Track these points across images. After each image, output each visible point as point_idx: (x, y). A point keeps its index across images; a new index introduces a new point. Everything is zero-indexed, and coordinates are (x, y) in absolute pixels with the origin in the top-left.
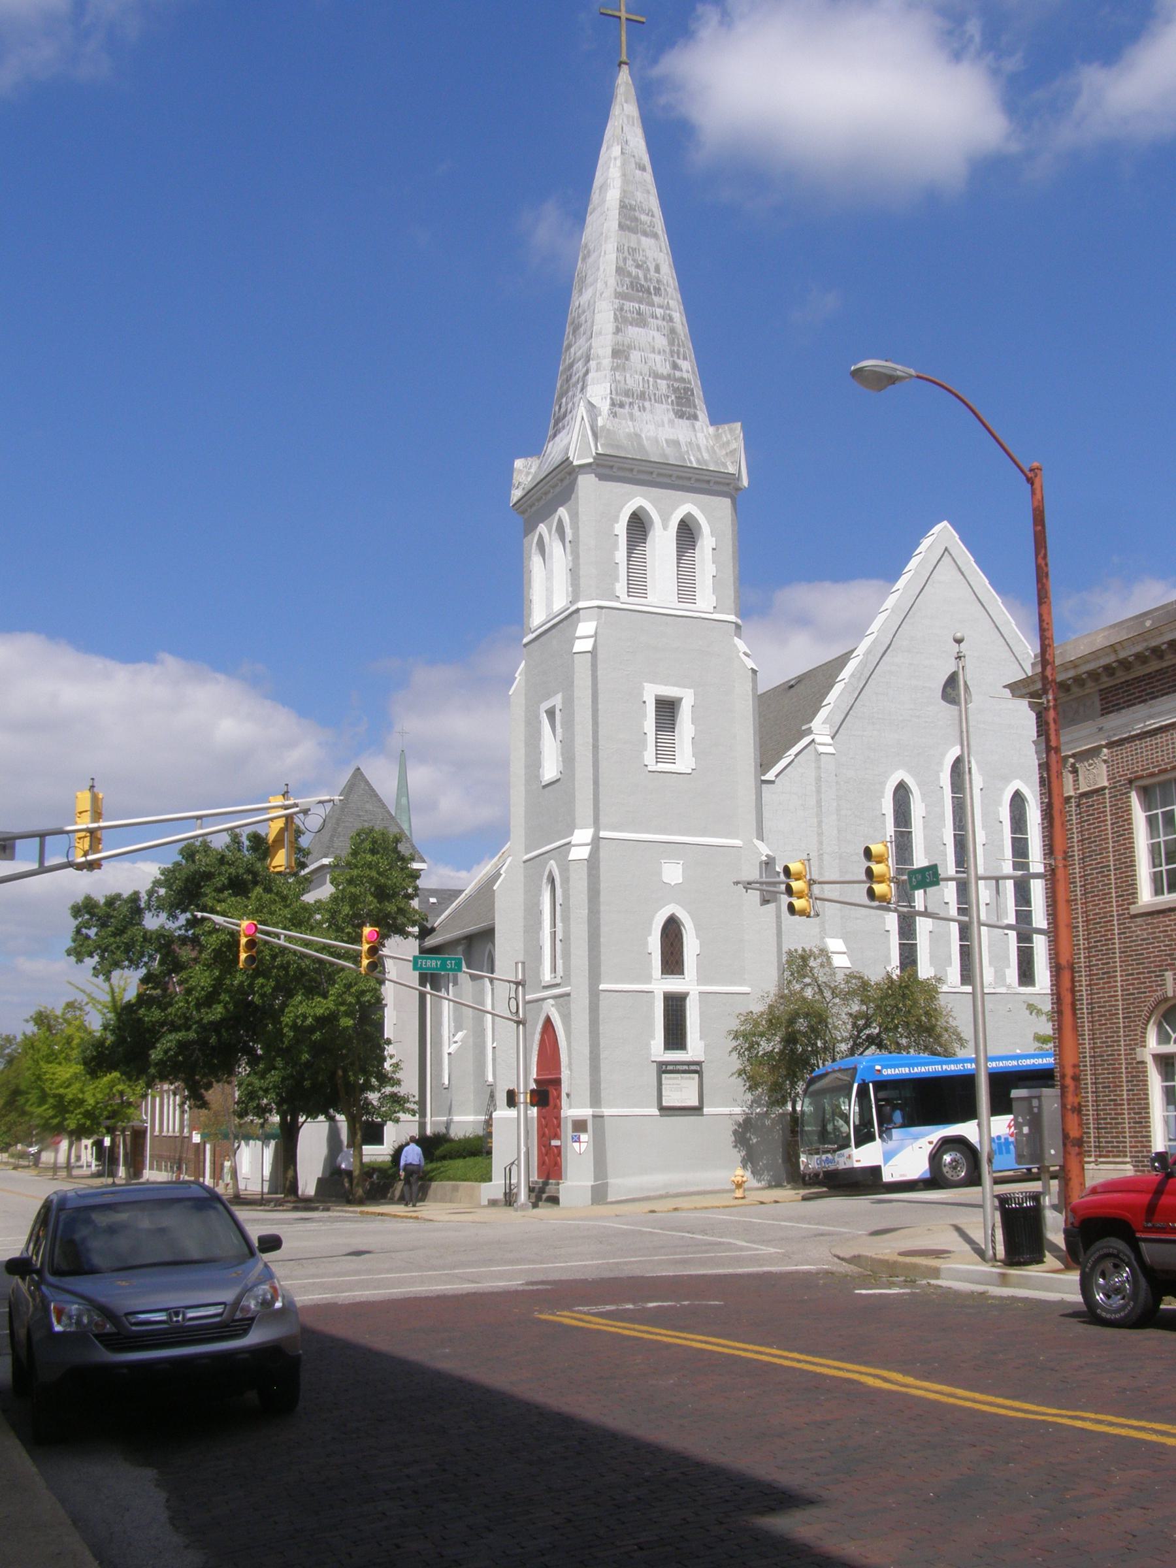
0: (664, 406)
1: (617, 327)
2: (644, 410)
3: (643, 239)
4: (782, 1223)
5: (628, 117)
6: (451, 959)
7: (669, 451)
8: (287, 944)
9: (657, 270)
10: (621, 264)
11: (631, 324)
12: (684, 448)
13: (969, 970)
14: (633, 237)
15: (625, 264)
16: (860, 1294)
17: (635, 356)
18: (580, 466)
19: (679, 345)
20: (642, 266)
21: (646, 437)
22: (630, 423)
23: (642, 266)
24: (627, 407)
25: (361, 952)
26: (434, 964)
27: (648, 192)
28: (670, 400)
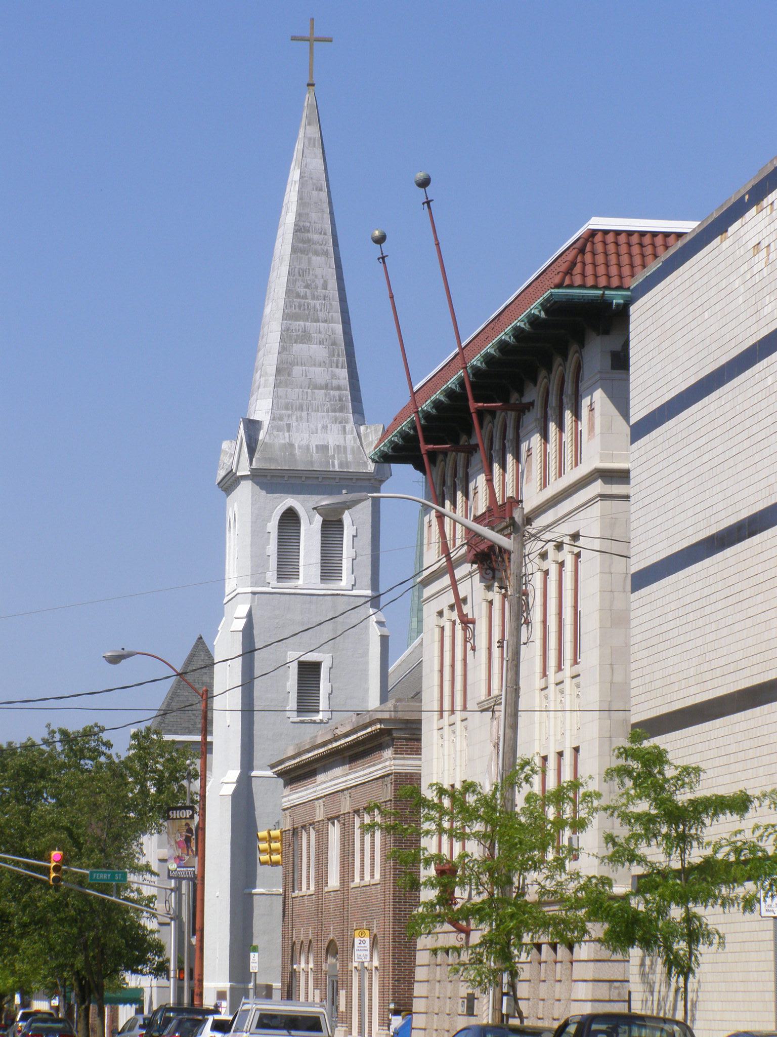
0: (320, 414)
1: (283, 347)
2: (301, 420)
3: (314, 258)
5: (310, 139)
7: (316, 456)
9: (325, 287)
11: (296, 342)
12: (331, 452)
14: (305, 258)
17: (297, 370)
18: (242, 476)
21: (299, 446)
22: (287, 434)
24: (286, 419)
26: (105, 876)
28: (325, 408)
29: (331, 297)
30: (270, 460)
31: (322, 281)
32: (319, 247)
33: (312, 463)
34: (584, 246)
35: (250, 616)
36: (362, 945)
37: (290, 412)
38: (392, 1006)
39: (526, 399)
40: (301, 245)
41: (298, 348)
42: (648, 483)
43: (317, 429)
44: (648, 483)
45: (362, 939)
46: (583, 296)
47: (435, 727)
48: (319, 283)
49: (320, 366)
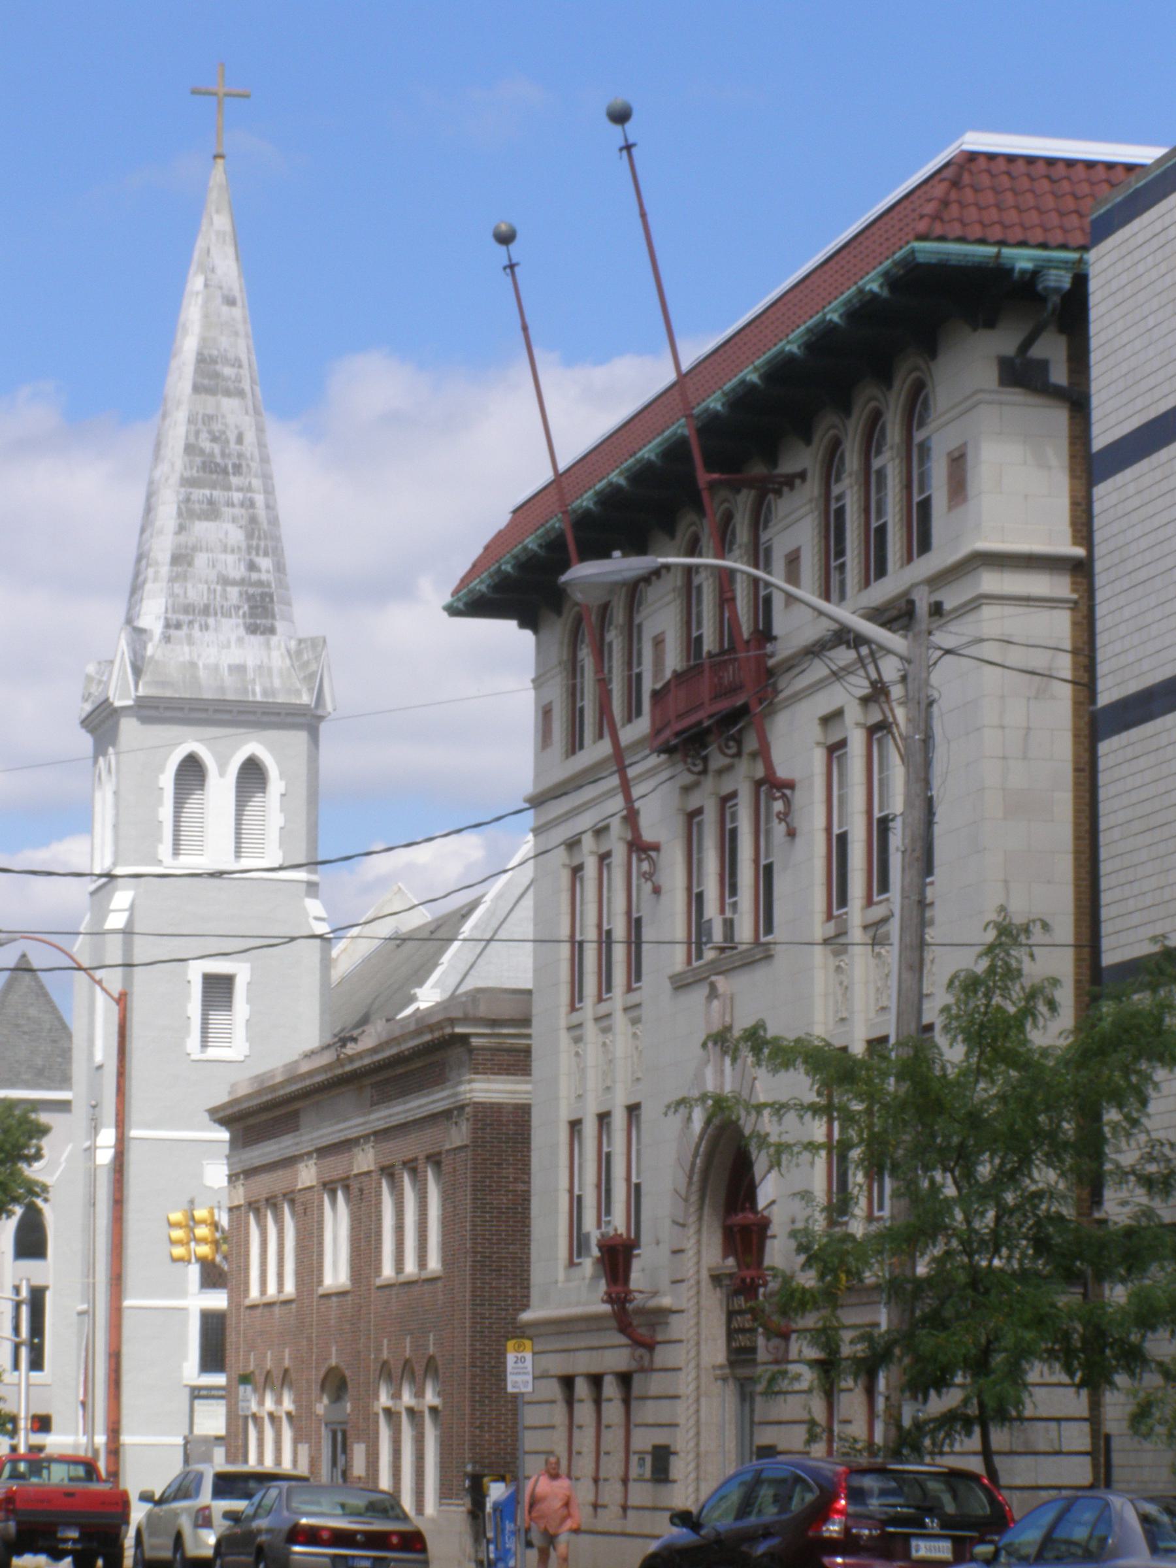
7: (229, 680)
9: (240, 439)
11: (199, 519)
12: (250, 675)
14: (211, 400)
17: (201, 559)
22: (186, 649)
28: (241, 612)
29: (248, 455)
30: (163, 684)
31: (236, 432)
32: (231, 385)
33: (222, 689)
34: (959, 176)
35: (132, 908)
36: (520, 1365)
37: (191, 617)
38: (469, 1468)
39: (787, 467)
40: (206, 382)
41: (202, 529)
42: (1144, 543)
43: (229, 642)
44: (1144, 543)
45: (520, 1355)
46: (966, 255)
47: (563, 1023)
48: (232, 436)
49: (233, 551)
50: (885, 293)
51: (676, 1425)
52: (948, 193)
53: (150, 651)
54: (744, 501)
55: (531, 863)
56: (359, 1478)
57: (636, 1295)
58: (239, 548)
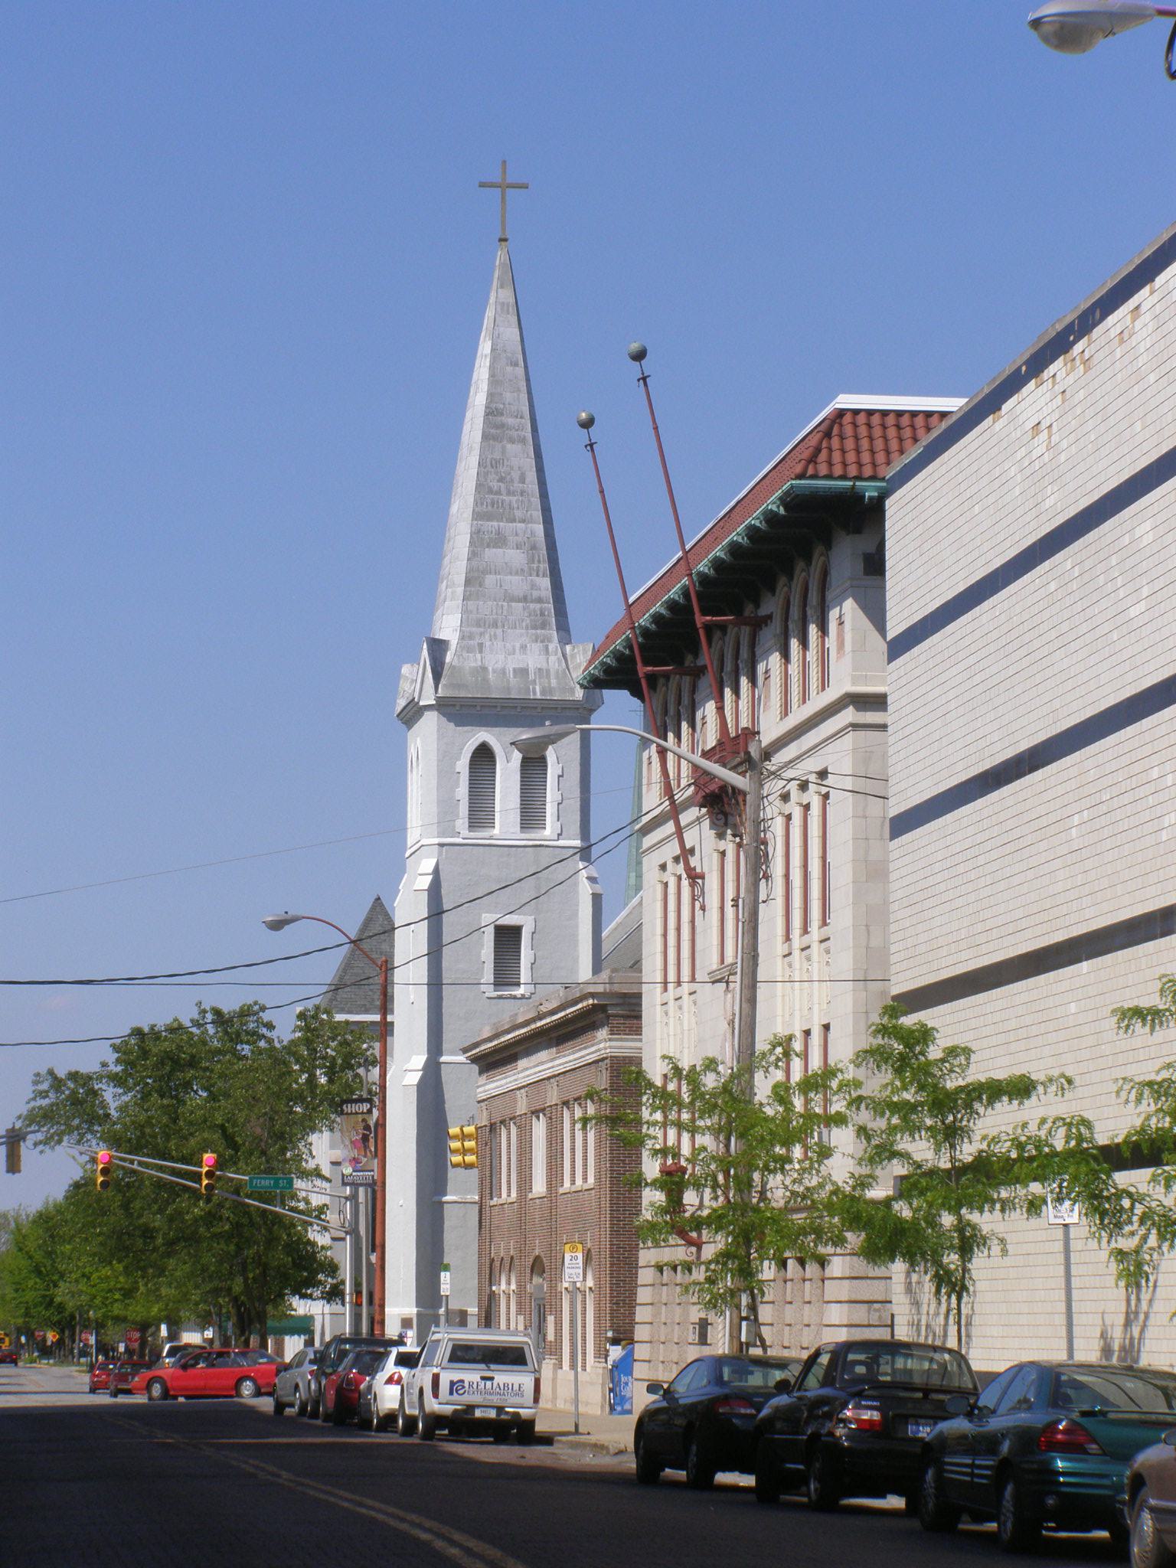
1: (473, 551)
2: (496, 639)
3: (509, 446)
4: (211, 1441)
6: (283, 1179)
8: (140, 1168)
9: (522, 480)
10: (482, 479)
11: (488, 546)
12: (532, 677)
13: (355, 1314)
15: (486, 480)
16: (790, 1469)
17: (490, 580)
19: (539, 562)
20: (504, 478)
21: (493, 669)
22: (478, 656)
23: (504, 478)
24: (477, 637)
25: (201, 1173)
27: (519, 390)
28: (524, 624)
29: (530, 492)
30: (459, 686)
34: (831, 428)
35: (436, 872)
37: (482, 630)
38: (610, 1334)
39: (763, 611)
44: (908, 709)
45: (573, 1255)
48: (516, 475)
49: (517, 573)
50: (782, 511)
51: (890, 1302)
52: (821, 442)
53: (448, 659)
54: (746, 630)
55: (396, 965)
56: (551, 1342)
57: (688, 1207)
58: (522, 570)
